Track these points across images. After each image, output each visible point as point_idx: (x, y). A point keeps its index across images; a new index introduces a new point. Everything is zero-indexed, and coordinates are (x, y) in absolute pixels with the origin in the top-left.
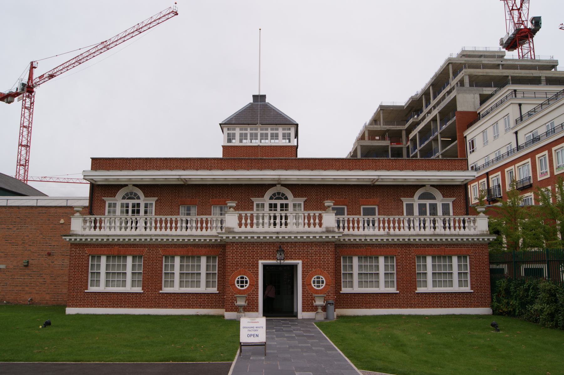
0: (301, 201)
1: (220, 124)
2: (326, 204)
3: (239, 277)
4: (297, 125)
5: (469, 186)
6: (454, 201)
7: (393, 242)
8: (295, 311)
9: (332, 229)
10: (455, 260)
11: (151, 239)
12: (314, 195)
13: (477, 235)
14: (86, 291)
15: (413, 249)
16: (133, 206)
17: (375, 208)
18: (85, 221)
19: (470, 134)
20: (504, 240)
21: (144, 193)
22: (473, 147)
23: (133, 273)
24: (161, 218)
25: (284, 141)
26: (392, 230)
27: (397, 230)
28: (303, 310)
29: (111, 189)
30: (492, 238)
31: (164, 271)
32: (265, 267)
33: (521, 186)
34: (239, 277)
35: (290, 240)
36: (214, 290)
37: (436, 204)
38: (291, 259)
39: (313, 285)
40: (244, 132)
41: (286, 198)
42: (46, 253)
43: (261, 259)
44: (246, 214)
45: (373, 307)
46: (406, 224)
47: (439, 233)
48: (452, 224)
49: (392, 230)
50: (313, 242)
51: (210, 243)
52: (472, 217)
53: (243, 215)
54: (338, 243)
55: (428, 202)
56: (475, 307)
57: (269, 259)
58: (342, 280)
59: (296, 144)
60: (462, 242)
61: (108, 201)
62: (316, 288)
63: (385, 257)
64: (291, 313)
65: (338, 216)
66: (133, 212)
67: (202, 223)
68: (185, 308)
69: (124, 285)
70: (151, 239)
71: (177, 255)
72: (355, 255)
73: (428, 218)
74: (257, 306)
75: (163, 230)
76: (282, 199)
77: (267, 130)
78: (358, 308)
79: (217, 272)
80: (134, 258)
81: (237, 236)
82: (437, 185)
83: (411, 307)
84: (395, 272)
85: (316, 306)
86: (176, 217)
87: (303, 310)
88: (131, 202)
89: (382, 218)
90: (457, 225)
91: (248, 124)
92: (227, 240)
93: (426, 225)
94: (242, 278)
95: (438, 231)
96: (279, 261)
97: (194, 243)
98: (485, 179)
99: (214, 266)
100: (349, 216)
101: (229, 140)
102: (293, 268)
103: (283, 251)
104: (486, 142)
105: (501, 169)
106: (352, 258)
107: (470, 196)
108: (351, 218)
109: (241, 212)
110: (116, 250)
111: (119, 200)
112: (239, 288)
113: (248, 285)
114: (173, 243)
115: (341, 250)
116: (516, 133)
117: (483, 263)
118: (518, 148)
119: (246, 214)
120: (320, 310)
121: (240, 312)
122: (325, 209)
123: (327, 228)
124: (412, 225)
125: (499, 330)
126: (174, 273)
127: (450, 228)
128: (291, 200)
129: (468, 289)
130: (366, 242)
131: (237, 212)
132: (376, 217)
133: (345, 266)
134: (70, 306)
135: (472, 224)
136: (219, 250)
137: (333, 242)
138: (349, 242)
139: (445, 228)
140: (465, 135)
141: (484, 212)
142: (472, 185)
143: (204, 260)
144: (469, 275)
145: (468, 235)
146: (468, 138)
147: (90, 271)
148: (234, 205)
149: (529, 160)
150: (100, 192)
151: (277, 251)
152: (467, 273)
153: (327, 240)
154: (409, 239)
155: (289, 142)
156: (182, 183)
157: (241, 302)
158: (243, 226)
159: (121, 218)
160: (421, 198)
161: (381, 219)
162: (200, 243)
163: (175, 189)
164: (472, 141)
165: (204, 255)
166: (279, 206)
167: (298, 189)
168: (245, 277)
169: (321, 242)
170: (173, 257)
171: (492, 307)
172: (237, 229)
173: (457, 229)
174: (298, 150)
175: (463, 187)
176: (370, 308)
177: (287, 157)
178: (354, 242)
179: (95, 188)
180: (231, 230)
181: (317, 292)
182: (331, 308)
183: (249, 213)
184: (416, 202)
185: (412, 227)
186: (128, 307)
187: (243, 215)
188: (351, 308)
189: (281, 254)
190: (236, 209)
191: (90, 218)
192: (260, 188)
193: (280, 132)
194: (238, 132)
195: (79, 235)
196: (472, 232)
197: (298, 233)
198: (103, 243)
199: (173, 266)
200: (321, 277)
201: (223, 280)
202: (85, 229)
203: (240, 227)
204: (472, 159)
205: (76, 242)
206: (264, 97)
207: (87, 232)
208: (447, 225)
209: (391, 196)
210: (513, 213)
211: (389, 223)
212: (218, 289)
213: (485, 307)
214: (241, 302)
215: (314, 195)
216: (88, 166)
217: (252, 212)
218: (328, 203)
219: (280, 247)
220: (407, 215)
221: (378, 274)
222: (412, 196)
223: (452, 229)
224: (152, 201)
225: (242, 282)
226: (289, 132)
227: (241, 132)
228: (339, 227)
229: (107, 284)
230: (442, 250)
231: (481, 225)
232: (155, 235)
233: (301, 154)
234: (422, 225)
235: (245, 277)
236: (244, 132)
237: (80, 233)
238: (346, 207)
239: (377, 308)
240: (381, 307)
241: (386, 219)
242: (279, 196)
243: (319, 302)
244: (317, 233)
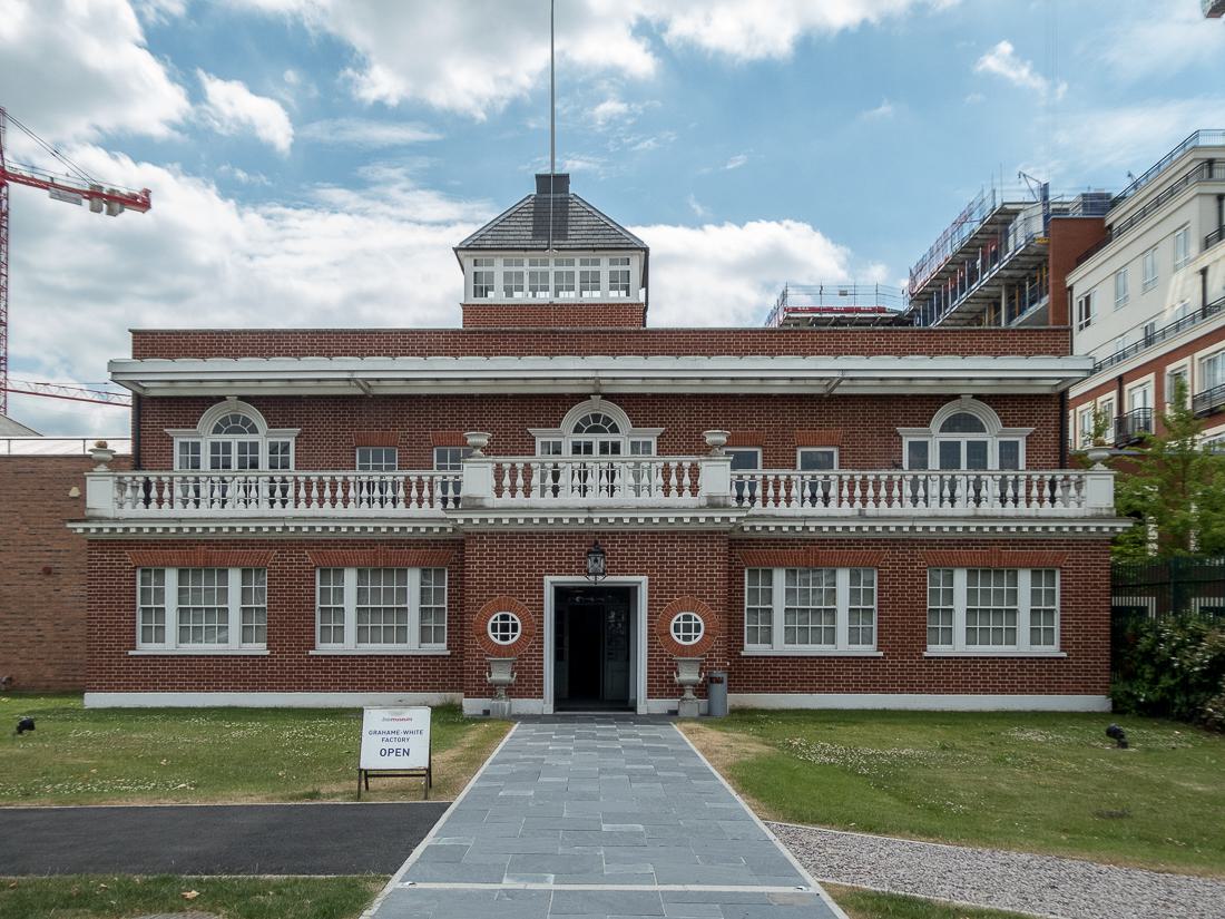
0: (651, 435)
1: (456, 250)
2: (709, 439)
3: (498, 614)
4: (646, 250)
5: (1071, 412)
6: (1031, 435)
7: (872, 535)
8: (632, 697)
9: (721, 500)
10: (1025, 579)
11: (285, 528)
12: (678, 418)
13: (1084, 519)
14: (131, 653)
15: (919, 552)
16: (242, 446)
17: (832, 453)
18: (121, 485)
19: (1083, 280)
20: (1153, 534)
21: (267, 417)
22: (1088, 315)
23: (850, 610)
24: (308, 478)
25: (613, 294)
26: (871, 505)
27: (883, 504)
28: (650, 696)
29: (187, 407)
30: (1121, 526)
31: (318, 605)
32: (562, 593)
33: (1205, 407)
34: (498, 614)
35: (618, 527)
36: (441, 648)
37: (986, 443)
38: (623, 572)
39: (674, 635)
40: (514, 269)
41: (615, 429)
42: (40, 570)
43: (551, 572)
44: (513, 465)
45: (819, 690)
46: (908, 492)
47: (989, 514)
48: (1022, 491)
49: (871, 505)
50: (675, 532)
51: (430, 536)
52: (1073, 474)
53: (507, 466)
54: (737, 535)
55: (964, 438)
56: (1068, 692)
57: (570, 572)
58: (746, 625)
59: (642, 300)
60: (1044, 536)
61: (179, 437)
62: (681, 642)
63: (969, 571)
64: (622, 704)
65: (740, 472)
66: (242, 466)
67: (408, 488)
68: (371, 690)
69: (402, 639)
70: (285, 528)
71: (350, 566)
72: (780, 565)
73: (964, 475)
74: (541, 685)
75: (315, 505)
76: (602, 430)
77: (571, 263)
78: (784, 691)
79: (446, 606)
80: (246, 572)
81: (491, 518)
82: (991, 396)
83: (911, 691)
84: (875, 606)
85: (681, 685)
86: (344, 473)
87: (650, 696)
88: (235, 440)
89: (846, 474)
90: (1035, 492)
91: (526, 250)
92: (468, 528)
93: (958, 492)
94: (504, 617)
95: (985, 508)
96: (592, 578)
97: (388, 537)
98: (1113, 394)
99: (439, 592)
100: (766, 472)
101: (480, 291)
102: (626, 595)
103: (603, 552)
104: (1121, 298)
105: (1156, 366)
106: (770, 572)
107: (1071, 436)
108: (771, 474)
109: (500, 459)
110: (202, 555)
111: (205, 436)
112: (498, 641)
113: (518, 634)
114: (338, 536)
115: (744, 553)
116: (1204, 272)
117: (1096, 586)
118: (1206, 311)
119: (513, 465)
120: (689, 694)
121: (500, 697)
122: (707, 450)
123: (709, 497)
124: (921, 492)
125: (1124, 745)
126: (406, 609)
127: (1016, 501)
128: (626, 435)
129: (1053, 650)
130: (806, 535)
131: (491, 458)
132: (834, 473)
133: (753, 592)
134: (93, 690)
135: (1073, 491)
136: (448, 554)
137: (725, 532)
138: (765, 535)
139: (1003, 500)
140: (1068, 285)
141: (1105, 462)
142: (1079, 409)
143: (414, 577)
144: (1057, 617)
145: (1062, 519)
146: (1078, 292)
147: (139, 605)
148: (484, 441)
149: (1151, 377)
150: (158, 414)
151: (589, 552)
152: (1052, 611)
153: (710, 526)
154: (912, 528)
155: (628, 294)
156: (360, 392)
157: (500, 675)
158: (506, 494)
159: (184, 478)
160: (949, 426)
161: (846, 478)
162: (403, 536)
163: (350, 409)
164: (1088, 299)
165: (414, 565)
166: (596, 449)
167: (643, 406)
168: (511, 614)
169: (695, 532)
170: (339, 572)
171: (1112, 695)
172: (492, 500)
173: (1035, 504)
174: (648, 313)
175: (1059, 402)
176: (811, 691)
177: (623, 329)
178: (778, 535)
179: (144, 406)
180: (478, 502)
181: (683, 651)
182: (718, 690)
183: (520, 461)
184: (935, 437)
185: (925, 498)
186: (235, 689)
187: (507, 466)
188: (766, 691)
189: (596, 561)
190: (487, 451)
191: (134, 478)
192: (549, 405)
193: (605, 269)
194: (498, 269)
195: (108, 519)
196: (1072, 510)
197: (639, 509)
198: (167, 537)
199: (340, 593)
200: (694, 615)
201: (460, 624)
202: (121, 505)
203: (499, 496)
204: (1083, 341)
205: (101, 537)
206: (563, 180)
207: (128, 511)
208: (1010, 492)
209: (866, 425)
210: (1180, 472)
211: (864, 489)
212: (448, 645)
213: (1095, 692)
214: (500, 675)
215: (678, 418)
216: (125, 353)
217: (527, 459)
218: (713, 437)
219: (596, 543)
220: (910, 468)
221: (951, 610)
222: (925, 422)
223: (1022, 503)
224: (288, 436)
225: (505, 628)
226: (625, 268)
227: (508, 269)
228: (740, 498)
229: (361, 635)
230: (993, 555)
231: (1099, 491)
232: (295, 518)
233: (655, 320)
234: (947, 492)
235: (511, 614)
236: (514, 269)
237: (111, 515)
238: (759, 451)
239: (829, 691)
240: (839, 691)
241: (858, 478)
242: (596, 424)
243: (688, 675)
244: (685, 509)
